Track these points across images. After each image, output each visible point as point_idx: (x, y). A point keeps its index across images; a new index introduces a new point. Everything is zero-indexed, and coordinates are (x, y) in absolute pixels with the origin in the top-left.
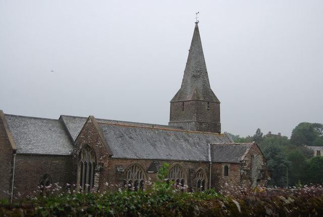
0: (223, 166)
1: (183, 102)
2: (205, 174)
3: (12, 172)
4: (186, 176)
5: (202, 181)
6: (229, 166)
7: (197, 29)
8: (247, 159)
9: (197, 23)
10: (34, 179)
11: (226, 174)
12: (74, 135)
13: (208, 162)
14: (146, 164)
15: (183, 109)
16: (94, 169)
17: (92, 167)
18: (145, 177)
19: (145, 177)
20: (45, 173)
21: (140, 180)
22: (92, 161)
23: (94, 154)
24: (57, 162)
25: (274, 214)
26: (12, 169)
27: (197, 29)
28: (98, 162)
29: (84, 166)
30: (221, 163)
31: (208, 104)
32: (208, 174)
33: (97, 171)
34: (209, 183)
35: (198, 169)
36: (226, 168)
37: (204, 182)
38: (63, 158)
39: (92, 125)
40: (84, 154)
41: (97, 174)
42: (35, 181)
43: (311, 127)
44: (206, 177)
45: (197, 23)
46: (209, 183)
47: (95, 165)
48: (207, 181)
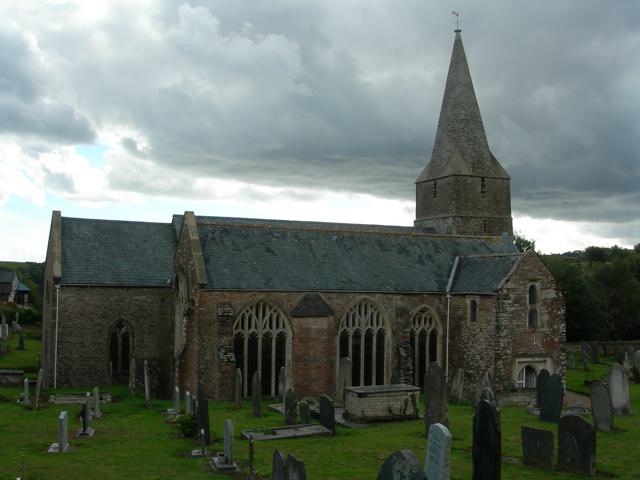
0: (468, 301)
2: (437, 317)
3: (54, 317)
4: (387, 318)
5: (418, 332)
6: (478, 300)
7: (458, 46)
8: (510, 285)
9: (458, 31)
10: (99, 328)
11: (474, 318)
14: (288, 301)
15: (435, 192)
18: (287, 324)
19: (287, 324)
20: (118, 318)
21: (275, 333)
24: (143, 297)
25: (588, 288)
26: (54, 312)
27: (458, 46)
30: (464, 295)
31: (483, 181)
32: (443, 318)
34: (444, 336)
35: (418, 309)
36: (474, 303)
37: (434, 335)
38: (155, 290)
39: (202, 221)
42: (100, 331)
43: (308, 422)
44: (439, 324)
45: (458, 31)
46: (444, 336)
48: (440, 332)
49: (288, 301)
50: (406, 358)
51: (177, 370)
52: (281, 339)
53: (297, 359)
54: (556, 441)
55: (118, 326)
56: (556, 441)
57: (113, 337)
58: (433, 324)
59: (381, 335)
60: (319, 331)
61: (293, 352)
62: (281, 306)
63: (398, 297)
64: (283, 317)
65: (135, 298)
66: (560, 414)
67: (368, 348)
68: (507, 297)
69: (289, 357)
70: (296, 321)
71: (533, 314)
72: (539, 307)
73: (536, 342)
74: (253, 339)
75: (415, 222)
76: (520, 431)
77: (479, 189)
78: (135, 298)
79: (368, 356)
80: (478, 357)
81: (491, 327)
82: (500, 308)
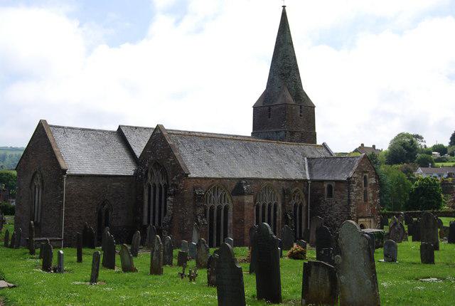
0: (326, 185)
1: (269, 107)
2: (303, 196)
4: (279, 199)
7: (284, 15)
8: (356, 175)
9: (284, 7)
11: (330, 195)
12: (138, 152)
13: (306, 180)
16: (166, 192)
17: (163, 189)
18: (230, 200)
19: (230, 200)
21: (223, 205)
22: (162, 182)
23: (164, 173)
27: (284, 15)
28: (171, 183)
29: (152, 188)
31: (301, 108)
33: (170, 195)
36: (330, 188)
40: (152, 173)
41: (170, 198)
47: (167, 187)
49: (231, 185)
50: (291, 220)
51: (34, 233)
52: (226, 209)
53: (236, 222)
54: (101, 262)
55: (102, 204)
56: (101, 262)
57: (100, 213)
58: (301, 200)
59: (276, 206)
60: (249, 204)
61: (234, 218)
62: (226, 189)
63: (284, 182)
64: (227, 195)
65: (113, 184)
66: (41, 250)
67: (219, 218)
68: (354, 182)
69: (230, 221)
70: (235, 198)
71: (366, 193)
72: (369, 190)
73: (367, 209)
74: (212, 208)
75: (252, 133)
76: (436, 260)
77: (299, 113)
78: (113, 184)
79: (219, 225)
80: (334, 219)
81: (345, 201)
82: (350, 189)
